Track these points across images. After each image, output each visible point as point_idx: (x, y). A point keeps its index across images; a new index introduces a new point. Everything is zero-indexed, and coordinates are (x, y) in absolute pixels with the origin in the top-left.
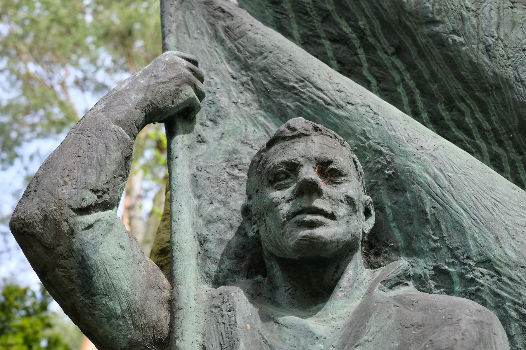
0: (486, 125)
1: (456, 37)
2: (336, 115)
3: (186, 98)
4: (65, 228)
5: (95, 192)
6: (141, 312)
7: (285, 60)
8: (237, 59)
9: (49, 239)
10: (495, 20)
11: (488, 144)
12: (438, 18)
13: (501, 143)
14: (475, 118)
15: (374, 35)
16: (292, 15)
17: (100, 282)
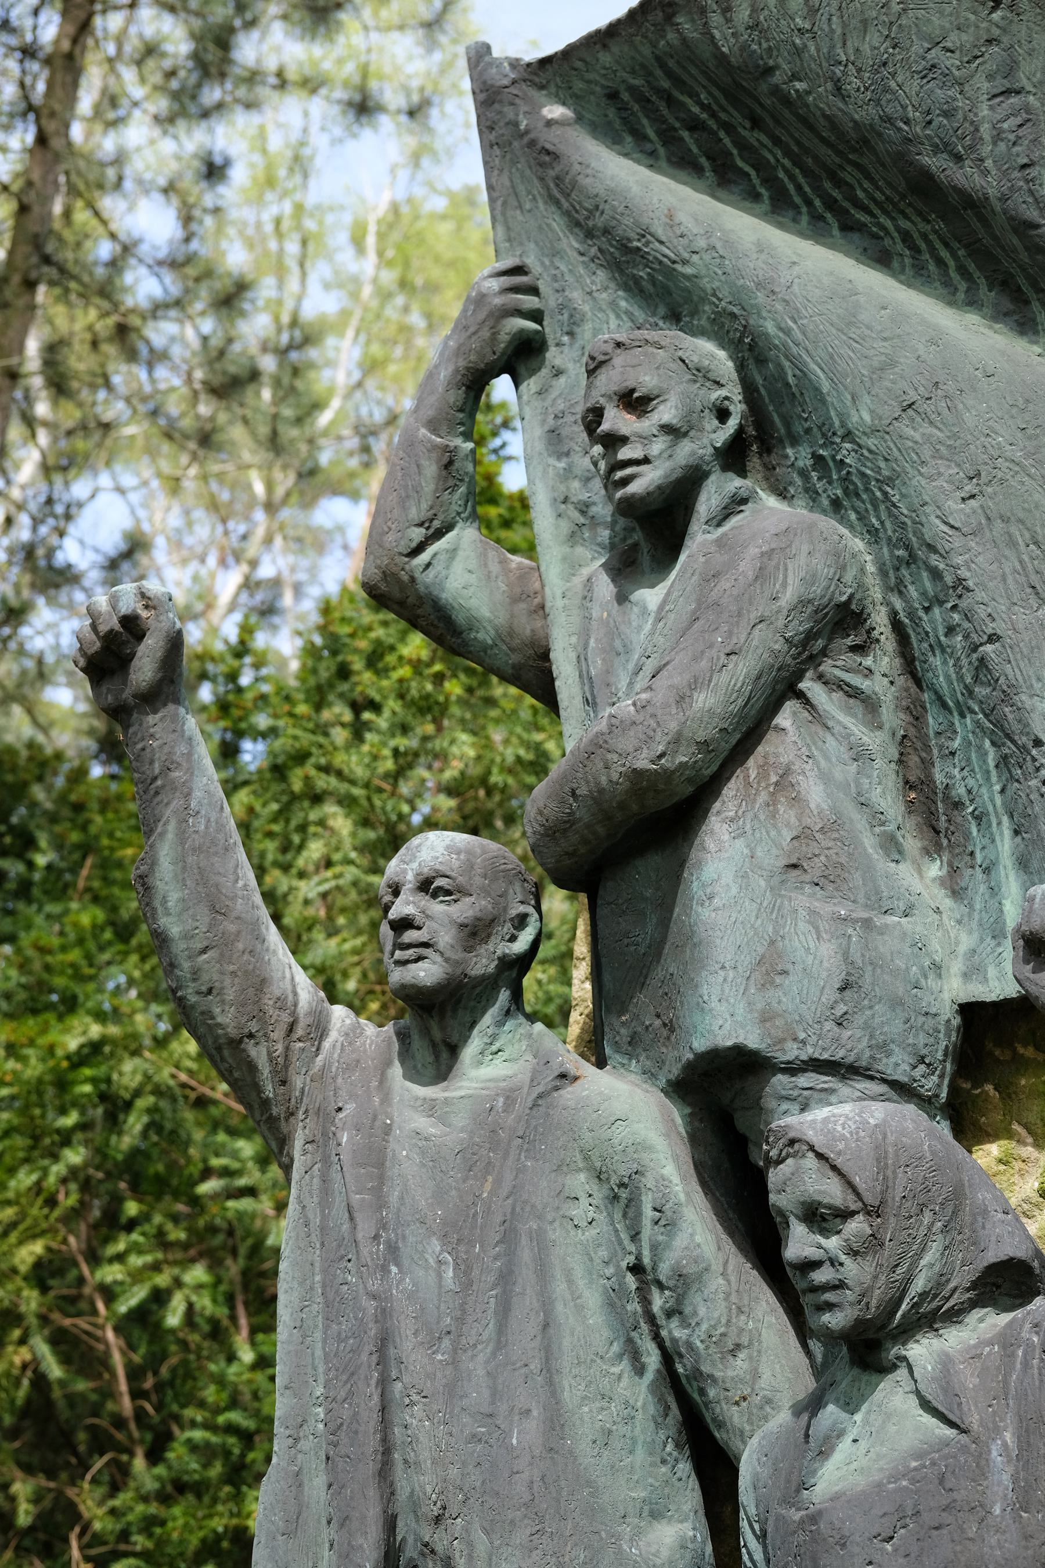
0: (878, 195)
1: (798, 85)
2: (684, 276)
3: (507, 338)
4: (406, 578)
5: (421, 525)
6: (511, 633)
7: (621, 209)
8: (578, 224)
9: (396, 594)
10: (839, 31)
11: (893, 219)
12: (771, 63)
13: (907, 217)
14: (865, 190)
15: (725, 110)
16: (636, 107)
17: (460, 618)
